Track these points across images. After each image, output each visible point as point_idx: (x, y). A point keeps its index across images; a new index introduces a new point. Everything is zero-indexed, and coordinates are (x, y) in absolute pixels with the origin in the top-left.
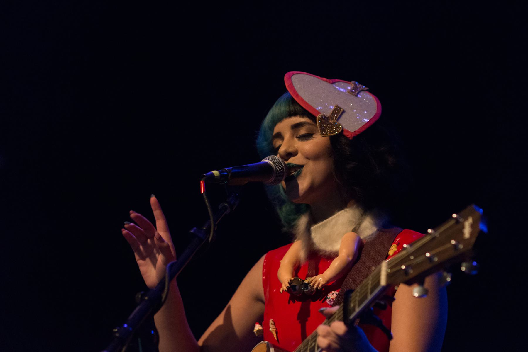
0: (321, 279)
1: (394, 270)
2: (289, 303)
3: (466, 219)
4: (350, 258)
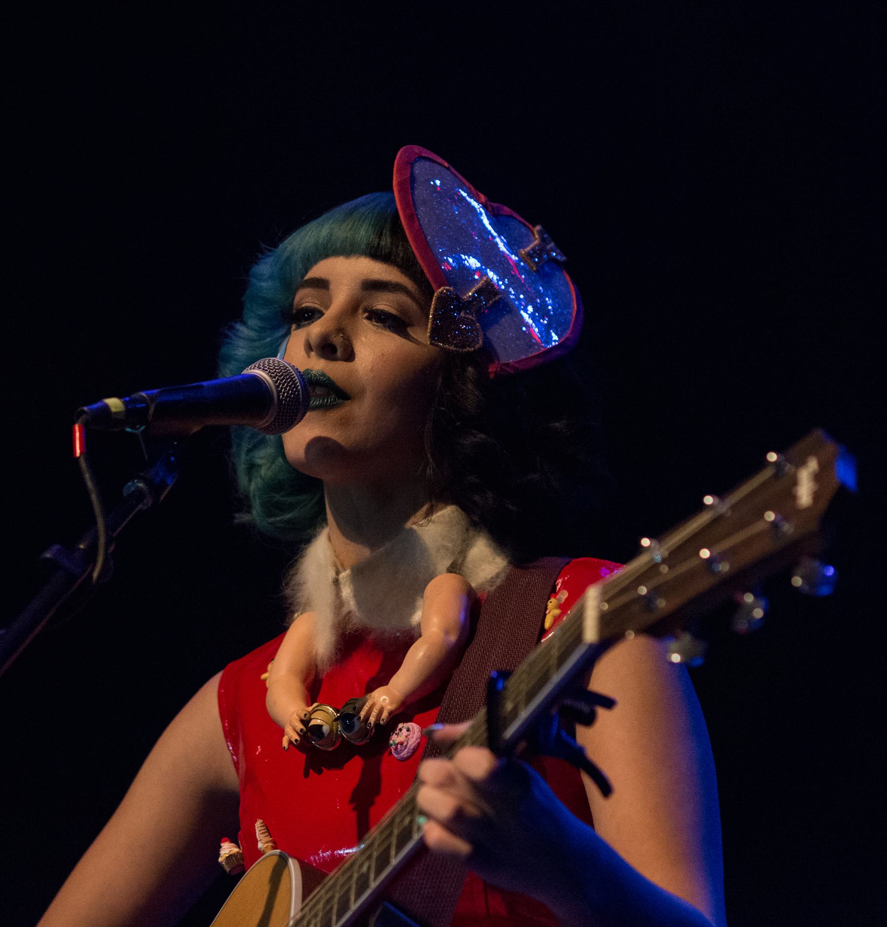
0: (384, 700)
1: (624, 599)
2: (306, 775)
3: (801, 463)
4: (453, 638)
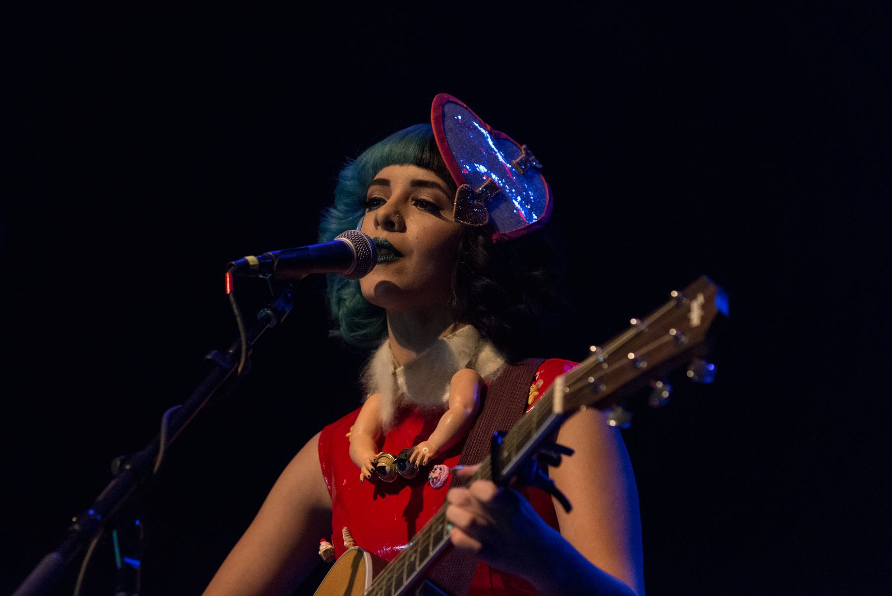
2: (375, 498)
3: (693, 297)
